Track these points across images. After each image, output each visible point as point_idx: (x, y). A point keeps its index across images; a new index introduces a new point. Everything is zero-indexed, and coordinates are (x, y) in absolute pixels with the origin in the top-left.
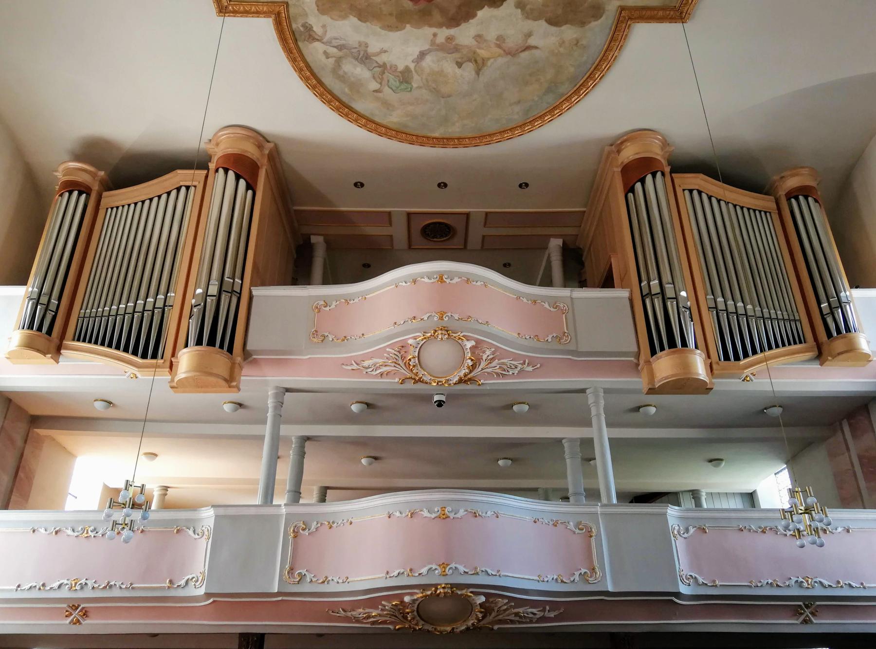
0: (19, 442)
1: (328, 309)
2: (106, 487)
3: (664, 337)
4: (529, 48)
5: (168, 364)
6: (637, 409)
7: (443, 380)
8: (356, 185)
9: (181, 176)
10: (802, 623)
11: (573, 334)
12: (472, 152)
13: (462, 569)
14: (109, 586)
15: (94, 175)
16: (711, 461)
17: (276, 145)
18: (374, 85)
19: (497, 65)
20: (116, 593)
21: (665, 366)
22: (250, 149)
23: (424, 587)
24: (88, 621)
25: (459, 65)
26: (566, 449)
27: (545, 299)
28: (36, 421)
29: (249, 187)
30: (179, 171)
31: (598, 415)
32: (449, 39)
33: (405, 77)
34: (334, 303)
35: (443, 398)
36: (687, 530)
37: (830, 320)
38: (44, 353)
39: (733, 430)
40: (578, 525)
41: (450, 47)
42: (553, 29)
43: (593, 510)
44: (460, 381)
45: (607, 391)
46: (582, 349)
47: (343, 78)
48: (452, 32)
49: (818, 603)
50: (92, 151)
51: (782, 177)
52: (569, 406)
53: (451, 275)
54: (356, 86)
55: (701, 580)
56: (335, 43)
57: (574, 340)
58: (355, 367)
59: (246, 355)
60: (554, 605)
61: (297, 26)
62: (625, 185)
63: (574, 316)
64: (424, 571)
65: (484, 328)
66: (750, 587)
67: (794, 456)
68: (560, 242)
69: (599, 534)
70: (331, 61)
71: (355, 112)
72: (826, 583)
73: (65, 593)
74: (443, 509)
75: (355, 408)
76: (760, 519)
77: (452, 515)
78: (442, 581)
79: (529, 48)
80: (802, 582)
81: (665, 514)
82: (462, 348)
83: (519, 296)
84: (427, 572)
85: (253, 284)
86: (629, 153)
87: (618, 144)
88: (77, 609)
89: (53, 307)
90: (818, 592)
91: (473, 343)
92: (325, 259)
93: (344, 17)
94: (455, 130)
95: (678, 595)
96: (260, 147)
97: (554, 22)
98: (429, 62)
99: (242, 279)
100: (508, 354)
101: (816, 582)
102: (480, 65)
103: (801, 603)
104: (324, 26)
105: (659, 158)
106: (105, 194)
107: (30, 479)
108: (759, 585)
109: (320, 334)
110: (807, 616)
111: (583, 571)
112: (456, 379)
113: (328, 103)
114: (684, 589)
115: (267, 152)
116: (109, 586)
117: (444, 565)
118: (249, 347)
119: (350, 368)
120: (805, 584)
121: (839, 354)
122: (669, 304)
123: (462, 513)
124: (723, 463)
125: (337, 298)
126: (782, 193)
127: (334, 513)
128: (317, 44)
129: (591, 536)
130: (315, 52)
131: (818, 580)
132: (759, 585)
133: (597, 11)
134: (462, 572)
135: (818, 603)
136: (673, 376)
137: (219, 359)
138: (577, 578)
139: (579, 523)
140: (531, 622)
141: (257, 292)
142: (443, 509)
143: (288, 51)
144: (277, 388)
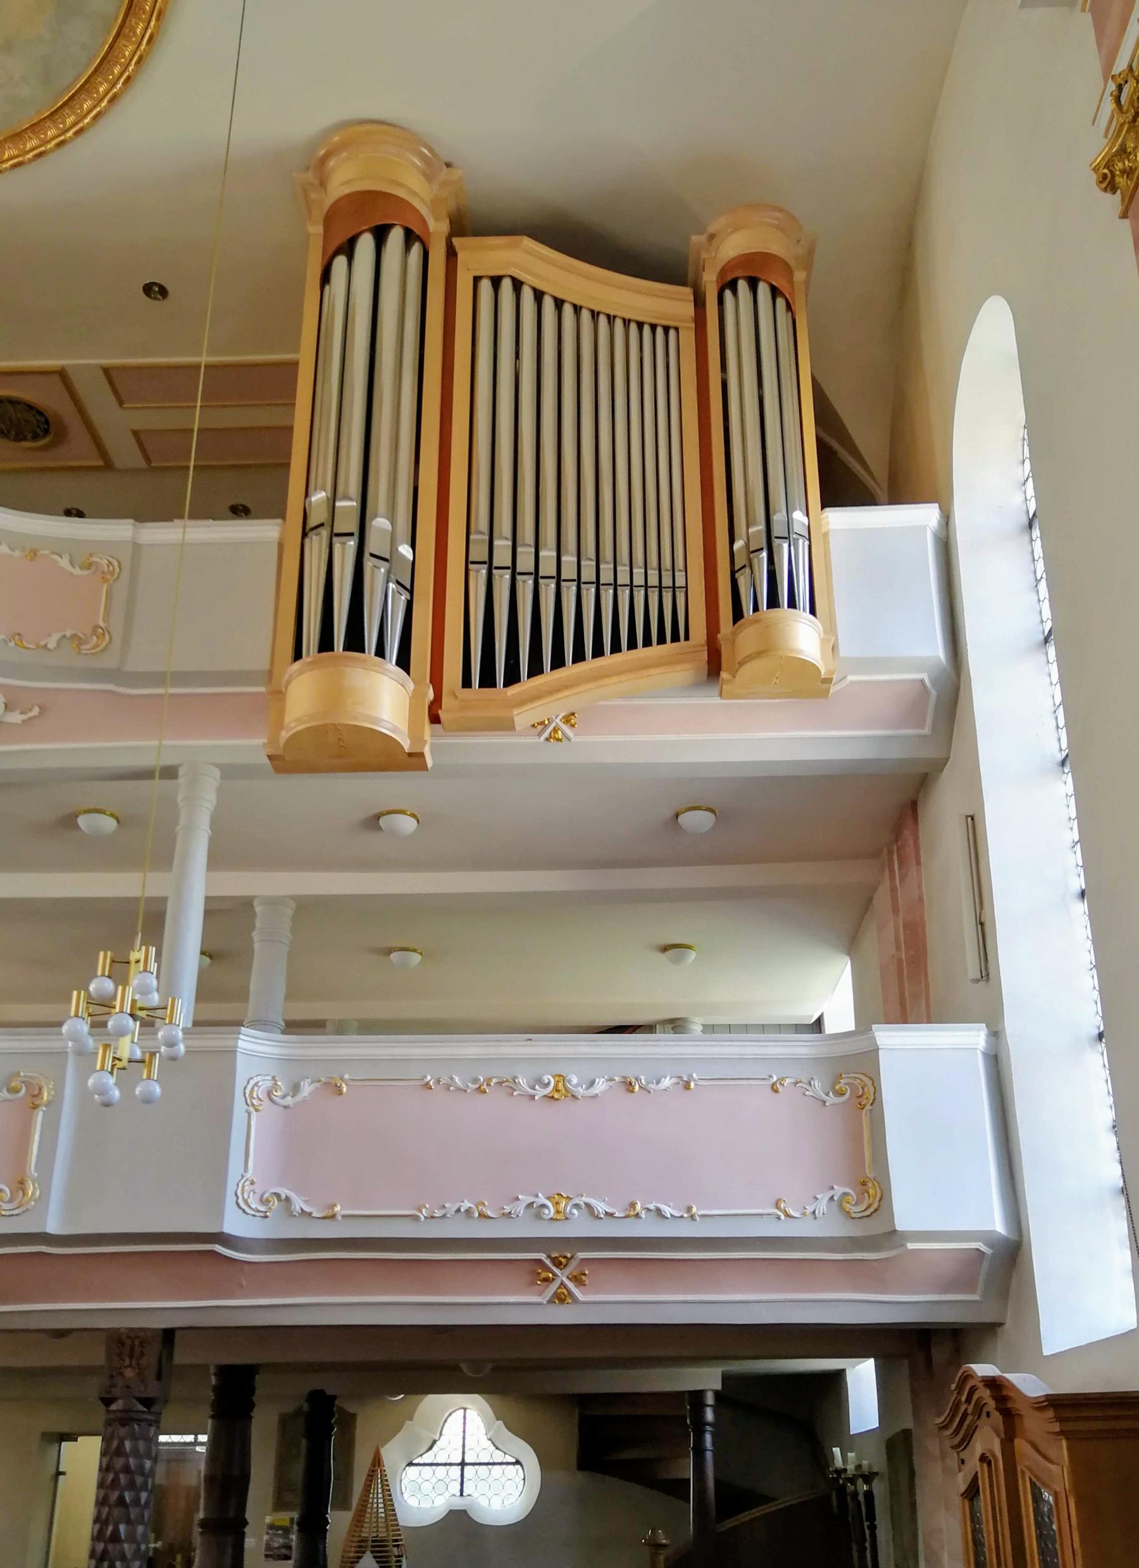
6: (373, 822)
8: (148, 289)
10: (551, 1302)
16: (665, 949)
36: (296, 1089)
45: (229, 772)
46: (133, 665)
49: (581, 1255)
51: (712, 237)
55: (298, 1204)
66: (415, 1218)
69: (55, 1104)
72: (601, 1207)
80: (544, 1206)
81: (232, 1052)
86: (345, 179)
90: (579, 1227)
101: (577, 1206)
103: (542, 1256)
108: (438, 1213)
110: (562, 1283)
114: (234, 1224)
124: (692, 955)
126: (710, 281)
129: (35, 1107)
131: (581, 1201)
132: (438, 1213)
135: (581, 1255)
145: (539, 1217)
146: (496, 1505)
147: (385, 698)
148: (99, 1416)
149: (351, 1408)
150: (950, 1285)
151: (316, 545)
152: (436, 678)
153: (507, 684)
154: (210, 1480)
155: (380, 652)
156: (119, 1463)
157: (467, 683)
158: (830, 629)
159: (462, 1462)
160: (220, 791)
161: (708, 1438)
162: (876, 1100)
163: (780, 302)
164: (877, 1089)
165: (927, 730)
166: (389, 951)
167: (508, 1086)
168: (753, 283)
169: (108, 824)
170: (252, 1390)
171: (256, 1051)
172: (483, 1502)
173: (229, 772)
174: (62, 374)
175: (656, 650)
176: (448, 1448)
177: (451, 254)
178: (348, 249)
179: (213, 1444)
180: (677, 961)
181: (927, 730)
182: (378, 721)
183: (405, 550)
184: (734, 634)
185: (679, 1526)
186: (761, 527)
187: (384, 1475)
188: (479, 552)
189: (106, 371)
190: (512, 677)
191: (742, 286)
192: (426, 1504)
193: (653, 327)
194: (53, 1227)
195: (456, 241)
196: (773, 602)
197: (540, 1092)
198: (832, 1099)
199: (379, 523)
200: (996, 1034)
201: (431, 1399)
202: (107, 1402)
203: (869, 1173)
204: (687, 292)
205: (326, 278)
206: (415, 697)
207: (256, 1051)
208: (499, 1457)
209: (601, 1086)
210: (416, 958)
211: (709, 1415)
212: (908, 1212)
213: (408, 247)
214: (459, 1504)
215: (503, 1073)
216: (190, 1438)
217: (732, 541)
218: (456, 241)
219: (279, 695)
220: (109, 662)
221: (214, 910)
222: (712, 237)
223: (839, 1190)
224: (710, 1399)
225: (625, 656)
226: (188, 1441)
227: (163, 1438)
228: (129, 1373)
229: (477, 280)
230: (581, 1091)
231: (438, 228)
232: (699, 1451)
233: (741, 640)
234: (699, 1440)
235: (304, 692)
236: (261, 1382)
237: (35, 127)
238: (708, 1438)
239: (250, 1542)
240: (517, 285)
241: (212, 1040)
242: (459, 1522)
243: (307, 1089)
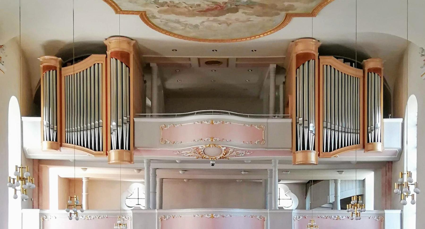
1: (166, 128)
2: (60, 178)
3: (299, 145)
5: (105, 153)
7: (214, 158)
9: (93, 59)
11: (266, 139)
12: (227, 43)
17: (136, 41)
21: (300, 156)
27: (256, 124)
29: (127, 66)
31: (275, 171)
34: (169, 126)
35: (214, 162)
36: (300, 217)
37: (370, 134)
44: (221, 158)
53: (216, 120)
57: (266, 143)
58: (178, 153)
62: (296, 66)
65: (229, 143)
67: (375, 170)
68: (275, 66)
74: (212, 215)
76: (326, 213)
77: (215, 217)
82: (221, 150)
83: (245, 123)
85: (135, 116)
91: (225, 148)
92: (155, 53)
94: (220, 37)
96: (129, 43)
100: (239, 150)
105: (312, 52)
106: (63, 69)
112: (219, 157)
115: (132, 44)
118: (136, 146)
119: (176, 153)
121: (369, 151)
122: (305, 130)
123: (219, 216)
125: (170, 123)
126: (366, 69)
127: (174, 213)
136: (302, 161)
137: (126, 154)
141: (136, 120)
142: (212, 215)
144: (147, 160)
152: (319, 151)
158: (383, 145)
164: (384, 219)
165: (396, 157)
167: (331, 218)
177: (319, 59)
180: (341, 174)
188: (325, 126)
190: (331, 151)
195: (320, 57)
196: (374, 141)
197: (335, 218)
198: (378, 220)
200: (402, 211)
204: (362, 70)
206: (316, 154)
209: (344, 217)
217: (368, 127)
218: (320, 57)
230: (341, 218)
233: (370, 146)
243: (301, 217)
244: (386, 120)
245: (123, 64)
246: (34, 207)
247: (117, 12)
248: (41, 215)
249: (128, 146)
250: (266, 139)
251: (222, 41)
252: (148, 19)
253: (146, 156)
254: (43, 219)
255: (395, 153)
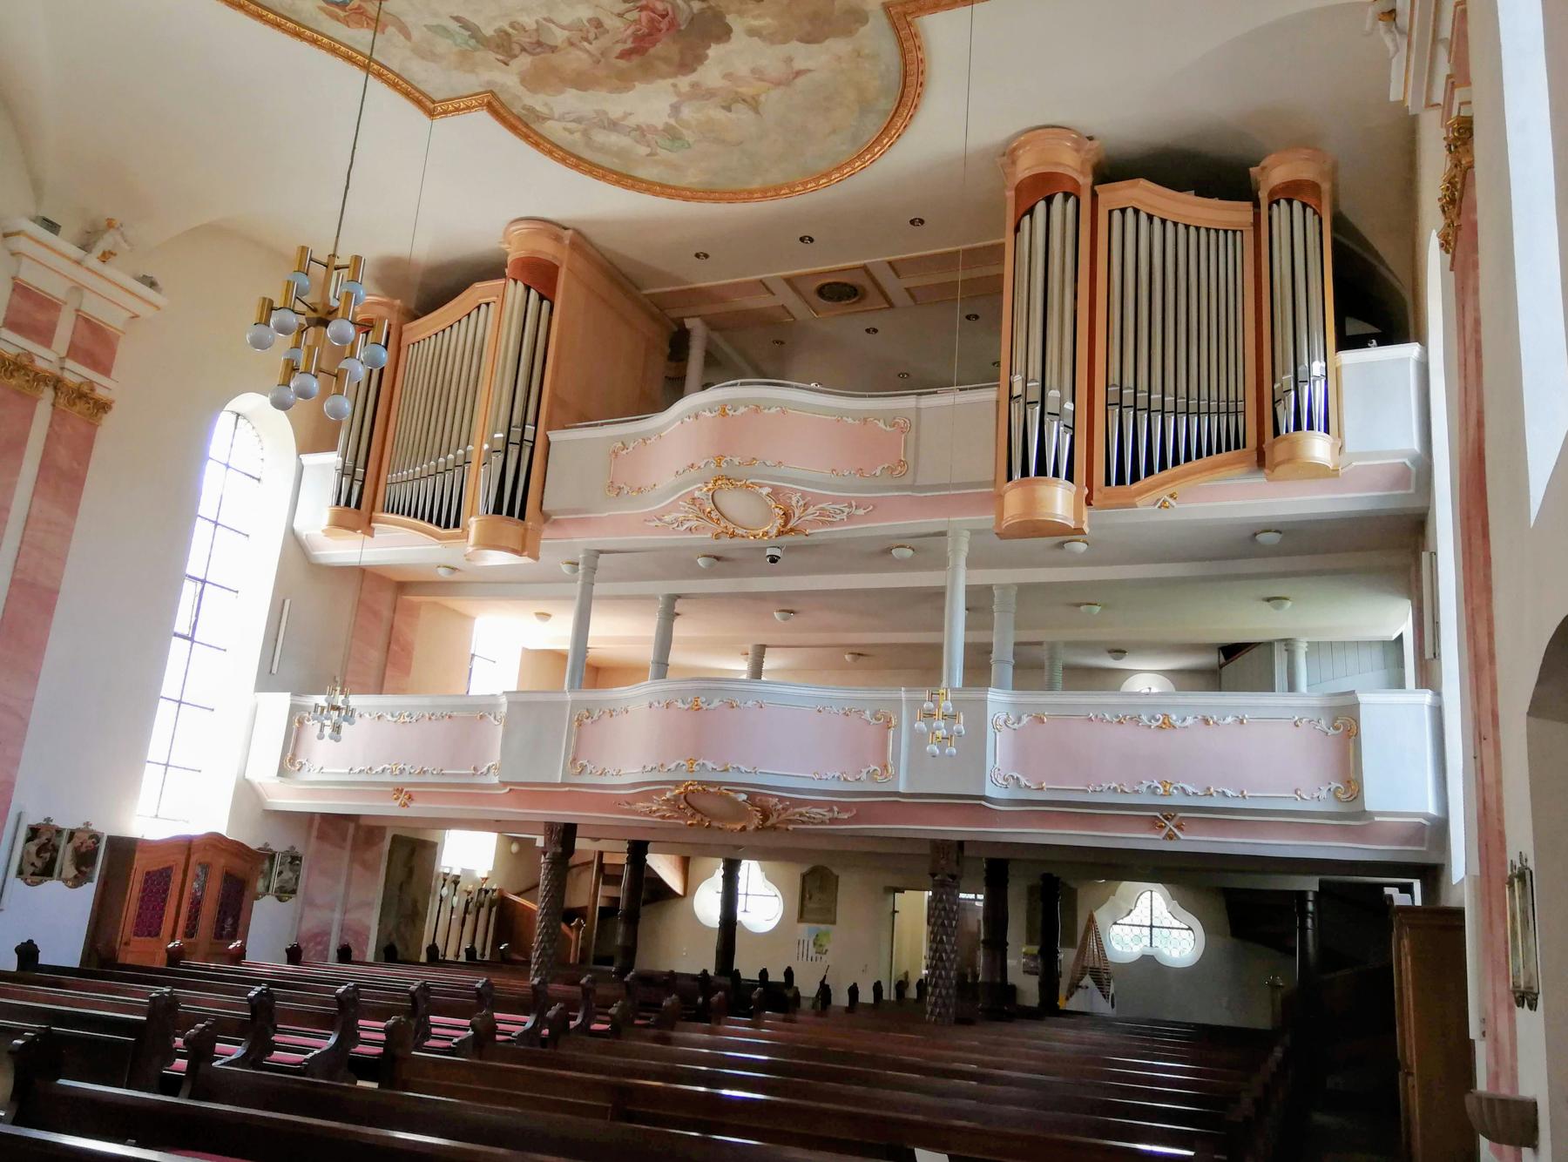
0: (386, 613)
2: (526, 651)
3: (1027, 462)
4: (798, 73)
11: (911, 461)
13: (710, 765)
14: (422, 772)
15: (390, 306)
16: (1268, 600)
17: (578, 232)
18: (643, 150)
19: (773, 100)
20: (429, 779)
22: (546, 249)
23: (677, 784)
24: (413, 805)
25: (728, 109)
26: (996, 600)
28: (402, 587)
30: (477, 285)
32: (694, 85)
33: (672, 134)
35: (777, 552)
36: (1019, 720)
38: (354, 530)
39: (1240, 562)
40: (874, 715)
41: (701, 94)
42: (815, 47)
43: (894, 695)
45: (974, 532)
46: (921, 481)
47: (602, 149)
48: (693, 77)
50: (393, 274)
51: (1263, 168)
52: (929, 551)
54: (621, 153)
55: (1023, 781)
56: (573, 116)
59: (545, 517)
60: (844, 807)
61: (517, 110)
63: (917, 438)
64: (673, 766)
70: (577, 136)
71: (642, 181)
72: (1190, 789)
73: (387, 778)
75: (701, 562)
77: (705, 706)
78: (689, 777)
79: (798, 73)
81: (985, 701)
82: (759, 495)
83: (842, 414)
84: (677, 770)
85: (549, 427)
86: (1026, 166)
87: (1009, 153)
88: (402, 792)
89: (359, 475)
90: (1177, 800)
93: (561, 92)
94: (775, 176)
95: (983, 798)
96: (558, 239)
97: (809, 39)
98: (687, 112)
99: (536, 425)
100: (825, 498)
102: (754, 104)
104: (546, 104)
107: (407, 650)
109: (616, 485)
111: (873, 767)
113: (603, 178)
114: (990, 791)
116: (422, 772)
117: (692, 761)
120: (1161, 791)
123: (716, 703)
124: (1289, 604)
126: (1263, 196)
128: (549, 123)
130: (553, 130)
133: (858, 17)
134: (710, 770)
137: (510, 527)
138: (864, 776)
139: (877, 712)
140: (823, 823)
141: (555, 436)
143: (526, 137)
144: (587, 551)
145: (1154, 793)
146: (1175, 954)
147: (1059, 500)
148: (930, 881)
149: (1074, 885)
150: (1407, 841)
151: (1017, 409)
152: (1090, 484)
153: (1132, 482)
154: (986, 918)
155: (1056, 474)
156: (940, 906)
157: (1108, 483)
159: (1149, 929)
160: (970, 543)
161: (1309, 921)
162: (1358, 734)
163: (1309, 211)
164: (1358, 727)
165: (1412, 491)
166: (1079, 605)
167: (1136, 720)
168: (1290, 202)
169: (908, 553)
170: (1007, 873)
171: (998, 700)
172: (1166, 952)
173: (974, 532)
174: (864, 268)
175: (1224, 455)
176: (1140, 914)
177: (1094, 196)
178: (1031, 211)
179: (988, 901)
180: (1277, 608)
181: (1412, 491)
182: (1056, 516)
183: (1069, 406)
184: (1273, 445)
185: (1289, 976)
186: (1291, 376)
187: (1097, 933)
188: (1114, 399)
189: (890, 263)
191: (1283, 202)
192: (1127, 950)
193: (1226, 231)
194: (902, 789)
196: (1298, 427)
198: (1332, 731)
199: (1053, 394)
201: (1125, 884)
202: (933, 875)
203: (1353, 776)
204: (1248, 205)
205: (1017, 229)
206: (1077, 494)
207: (998, 700)
208: (1176, 924)
209: (1190, 721)
210: (1097, 609)
211: (1310, 907)
212: (1374, 800)
213: (1066, 199)
214: (1149, 951)
215: (1133, 713)
216: (972, 896)
217: (1274, 381)
219: (1001, 497)
220: (908, 480)
221: (971, 591)
222: (1263, 168)
223: (1334, 785)
224: (1311, 897)
225: (1205, 459)
226: (974, 899)
227: (962, 896)
228: (943, 862)
229: (1110, 212)
230: (1178, 724)
231: (1085, 181)
232: (1304, 929)
233: (1278, 451)
234: (1303, 922)
235: (1013, 499)
236: (1012, 870)
237: (850, 163)
238: (1309, 921)
239: (1010, 962)
240: (1137, 212)
241: (973, 694)
242: (1148, 963)
243: (1025, 719)
244: (1350, 357)
245: (533, 292)
246: (1432, 859)
247: (431, 114)
248: (294, 709)
249: (514, 503)
250: (911, 461)
251: (791, 188)
252: (527, 125)
253: (581, 541)
254: (301, 722)
255: (1401, 476)
